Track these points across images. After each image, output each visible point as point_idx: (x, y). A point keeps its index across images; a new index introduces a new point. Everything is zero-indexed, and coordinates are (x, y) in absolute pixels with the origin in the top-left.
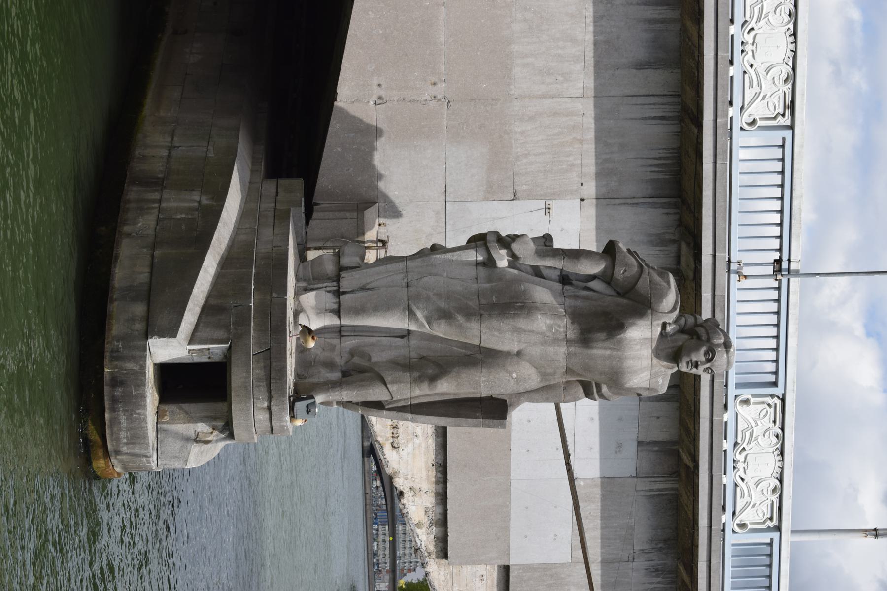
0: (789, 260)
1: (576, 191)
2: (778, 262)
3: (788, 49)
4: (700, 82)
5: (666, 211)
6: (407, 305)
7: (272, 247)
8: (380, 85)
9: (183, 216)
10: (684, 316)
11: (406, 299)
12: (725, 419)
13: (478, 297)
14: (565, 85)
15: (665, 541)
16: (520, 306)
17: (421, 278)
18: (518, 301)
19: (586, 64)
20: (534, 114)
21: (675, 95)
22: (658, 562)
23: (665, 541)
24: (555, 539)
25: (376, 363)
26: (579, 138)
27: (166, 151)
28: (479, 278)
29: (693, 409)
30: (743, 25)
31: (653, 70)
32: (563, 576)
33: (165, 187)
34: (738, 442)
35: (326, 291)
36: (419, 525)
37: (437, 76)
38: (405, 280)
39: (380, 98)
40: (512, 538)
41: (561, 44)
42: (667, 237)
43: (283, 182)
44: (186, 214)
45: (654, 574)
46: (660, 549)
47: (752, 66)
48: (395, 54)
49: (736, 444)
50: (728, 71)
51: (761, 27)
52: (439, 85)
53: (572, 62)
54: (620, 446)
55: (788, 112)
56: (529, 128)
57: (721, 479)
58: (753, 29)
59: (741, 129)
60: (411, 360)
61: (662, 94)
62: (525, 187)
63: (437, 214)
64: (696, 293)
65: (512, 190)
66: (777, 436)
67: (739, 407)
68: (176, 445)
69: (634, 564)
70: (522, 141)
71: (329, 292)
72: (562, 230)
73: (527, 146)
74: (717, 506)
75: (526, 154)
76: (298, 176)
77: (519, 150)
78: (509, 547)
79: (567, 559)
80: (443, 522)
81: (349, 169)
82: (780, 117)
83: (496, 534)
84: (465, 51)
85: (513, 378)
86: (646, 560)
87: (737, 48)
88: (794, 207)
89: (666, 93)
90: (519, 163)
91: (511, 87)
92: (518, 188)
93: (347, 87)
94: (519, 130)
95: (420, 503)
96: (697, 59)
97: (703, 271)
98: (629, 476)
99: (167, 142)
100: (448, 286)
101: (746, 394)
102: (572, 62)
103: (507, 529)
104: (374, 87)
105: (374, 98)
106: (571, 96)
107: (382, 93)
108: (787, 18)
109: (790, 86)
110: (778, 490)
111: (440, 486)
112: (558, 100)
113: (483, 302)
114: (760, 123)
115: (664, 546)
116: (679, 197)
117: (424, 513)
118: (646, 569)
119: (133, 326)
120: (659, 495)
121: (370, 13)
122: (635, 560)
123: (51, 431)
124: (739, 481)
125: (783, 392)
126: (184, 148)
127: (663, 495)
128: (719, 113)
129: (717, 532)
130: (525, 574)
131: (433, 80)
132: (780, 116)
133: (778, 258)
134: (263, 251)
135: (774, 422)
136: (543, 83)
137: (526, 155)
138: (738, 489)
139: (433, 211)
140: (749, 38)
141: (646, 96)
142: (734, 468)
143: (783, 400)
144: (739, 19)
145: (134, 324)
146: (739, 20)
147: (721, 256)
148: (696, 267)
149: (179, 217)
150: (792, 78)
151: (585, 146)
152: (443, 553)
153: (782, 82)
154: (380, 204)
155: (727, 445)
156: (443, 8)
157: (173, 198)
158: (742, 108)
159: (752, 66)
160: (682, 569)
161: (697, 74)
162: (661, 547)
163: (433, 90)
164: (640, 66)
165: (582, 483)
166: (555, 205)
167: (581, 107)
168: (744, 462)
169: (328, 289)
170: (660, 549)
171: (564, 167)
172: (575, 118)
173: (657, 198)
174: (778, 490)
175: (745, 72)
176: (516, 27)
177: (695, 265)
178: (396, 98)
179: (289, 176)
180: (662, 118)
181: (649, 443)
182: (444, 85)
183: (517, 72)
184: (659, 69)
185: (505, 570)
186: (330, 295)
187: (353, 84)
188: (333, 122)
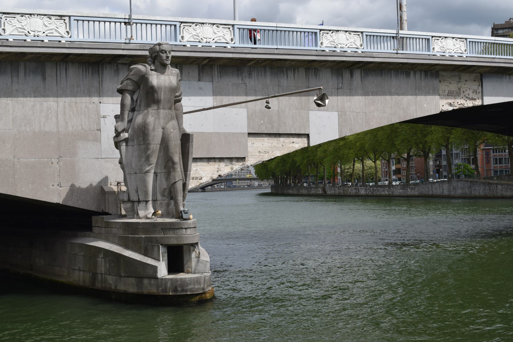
0: (277, 27)
2: (125, 23)
5: (105, 69)
8: (53, 185)
9: (108, 265)
11: (141, 174)
13: (140, 145)
14: (52, 109)
23: (238, 71)
26: (74, 104)
30: (27, 36)
32: (252, 111)
33: (96, 272)
36: (232, 169)
39: (58, 185)
41: (35, 111)
42: (115, 68)
45: (251, 75)
47: (44, 33)
49: (199, 42)
50: (46, 42)
51: (27, 28)
54: (200, 88)
55: (63, 18)
56: (70, 124)
58: (28, 32)
59: (70, 37)
62: (95, 126)
65: (96, 131)
71: (138, 205)
74: (59, 44)
76: (91, 218)
82: (65, 21)
89: (56, 68)
90: (85, 128)
92: (95, 129)
101: (179, 37)
103: (234, 134)
105: (58, 187)
107: (56, 184)
108: (24, 18)
109: (52, 17)
113: (142, 143)
114: (68, 30)
117: (227, 167)
121: (22, 189)
131: (50, 163)
134: (122, 232)
137: (82, 125)
140: (32, 33)
144: (24, 38)
148: (128, 57)
149: (108, 266)
150: (49, 16)
151: (78, 101)
153: (50, 20)
155: (200, 45)
158: (62, 37)
159: (44, 33)
160: (249, 64)
161: (48, 55)
164: (44, 79)
165: (215, 104)
166: (102, 114)
168: (35, 32)
169: (137, 205)
170: (241, 73)
171: (87, 110)
176: (28, 129)
178: (58, 179)
183: (47, 129)
185: (250, 134)
188: (68, 204)
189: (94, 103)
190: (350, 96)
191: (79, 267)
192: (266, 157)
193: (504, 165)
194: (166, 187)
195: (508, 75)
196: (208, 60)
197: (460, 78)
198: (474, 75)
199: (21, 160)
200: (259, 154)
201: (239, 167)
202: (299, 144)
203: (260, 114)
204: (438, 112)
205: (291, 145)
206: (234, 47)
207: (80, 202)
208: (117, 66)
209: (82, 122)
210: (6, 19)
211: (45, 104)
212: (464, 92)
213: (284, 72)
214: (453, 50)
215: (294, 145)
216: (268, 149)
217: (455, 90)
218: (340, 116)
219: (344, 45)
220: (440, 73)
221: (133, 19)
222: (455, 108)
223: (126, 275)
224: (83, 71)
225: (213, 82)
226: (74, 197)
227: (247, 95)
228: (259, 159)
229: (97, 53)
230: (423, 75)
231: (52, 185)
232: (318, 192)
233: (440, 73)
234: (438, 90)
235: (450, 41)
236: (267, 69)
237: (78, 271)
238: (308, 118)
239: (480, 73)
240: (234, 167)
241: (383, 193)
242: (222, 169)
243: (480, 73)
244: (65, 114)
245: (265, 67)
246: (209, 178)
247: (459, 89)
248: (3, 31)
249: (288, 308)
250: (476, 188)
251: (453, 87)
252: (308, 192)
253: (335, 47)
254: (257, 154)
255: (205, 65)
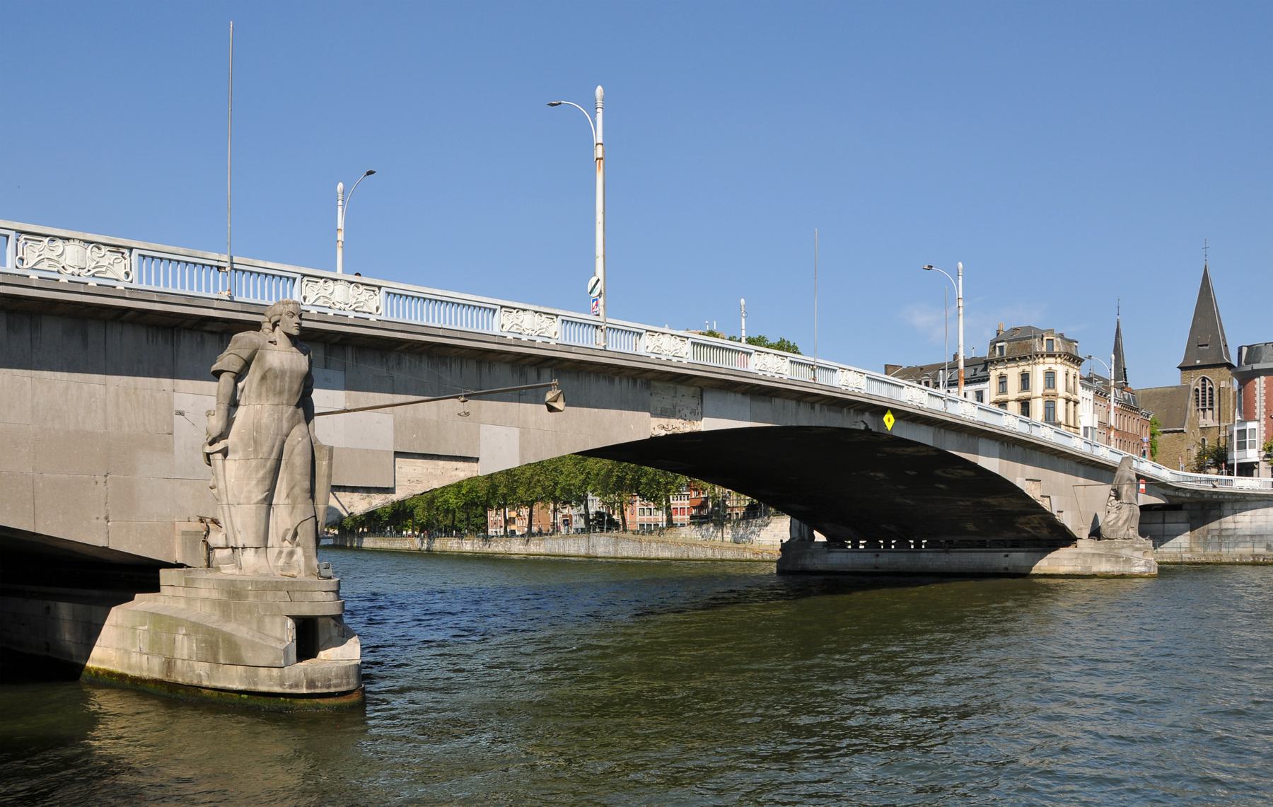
1: (168, 394)
5: (182, 337)
8: (98, 518)
9: (195, 645)
11: (249, 506)
12: (353, 317)
14: (98, 396)
25: (292, 526)
33: (173, 656)
36: (370, 503)
41: (69, 397)
42: (199, 339)
43: (162, 582)
44: (193, 643)
49: (330, 308)
52: (97, 480)
54: (326, 379)
55: (122, 250)
57: (539, 343)
58: (63, 267)
62: (165, 428)
65: (167, 436)
66: (326, 282)
67: (25, 266)
71: (242, 554)
72: (193, 405)
74: (110, 291)
76: (159, 573)
79: (391, 416)
80: (368, 490)
87: (76, 279)
103: (373, 451)
109: (102, 247)
110: (98, 245)
111: (347, 489)
113: (252, 456)
121: (48, 523)
123: (995, 675)
129: (132, 293)
134: (217, 595)
135: (511, 312)
142: (344, 310)
146: (56, 276)
152: (390, 490)
155: (331, 313)
156: (44, 474)
163: (101, 484)
165: (348, 404)
174: (98, 245)
175: (94, 276)
179: (158, 579)
180: (490, 367)
181: (326, 362)
185: (398, 454)
190: (536, 403)
192: (418, 488)
193: (645, 517)
195: (734, 392)
197: (676, 393)
198: (693, 389)
199: (45, 475)
202: (461, 472)
204: (649, 437)
205: (453, 473)
206: (380, 320)
207: (140, 546)
210: (26, 243)
211: (85, 387)
212: (679, 411)
213: (447, 364)
214: (349, 305)
215: (457, 473)
216: (421, 476)
217: (669, 407)
218: (522, 434)
219: (83, 272)
220: (653, 383)
222: (669, 433)
224: (148, 339)
226: (131, 537)
227: (393, 391)
230: (630, 381)
233: (653, 383)
234: (649, 406)
235: (850, 374)
236: (592, 375)
238: (479, 434)
239: (700, 387)
241: (497, 550)
242: (356, 504)
243: (700, 387)
245: (421, 354)
246: (336, 516)
247: (675, 407)
248: (21, 261)
249: (161, 768)
250: (624, 546)
251: (667, 403)
253: (520, 334)
254: (406, 484)
255: (336, 344)
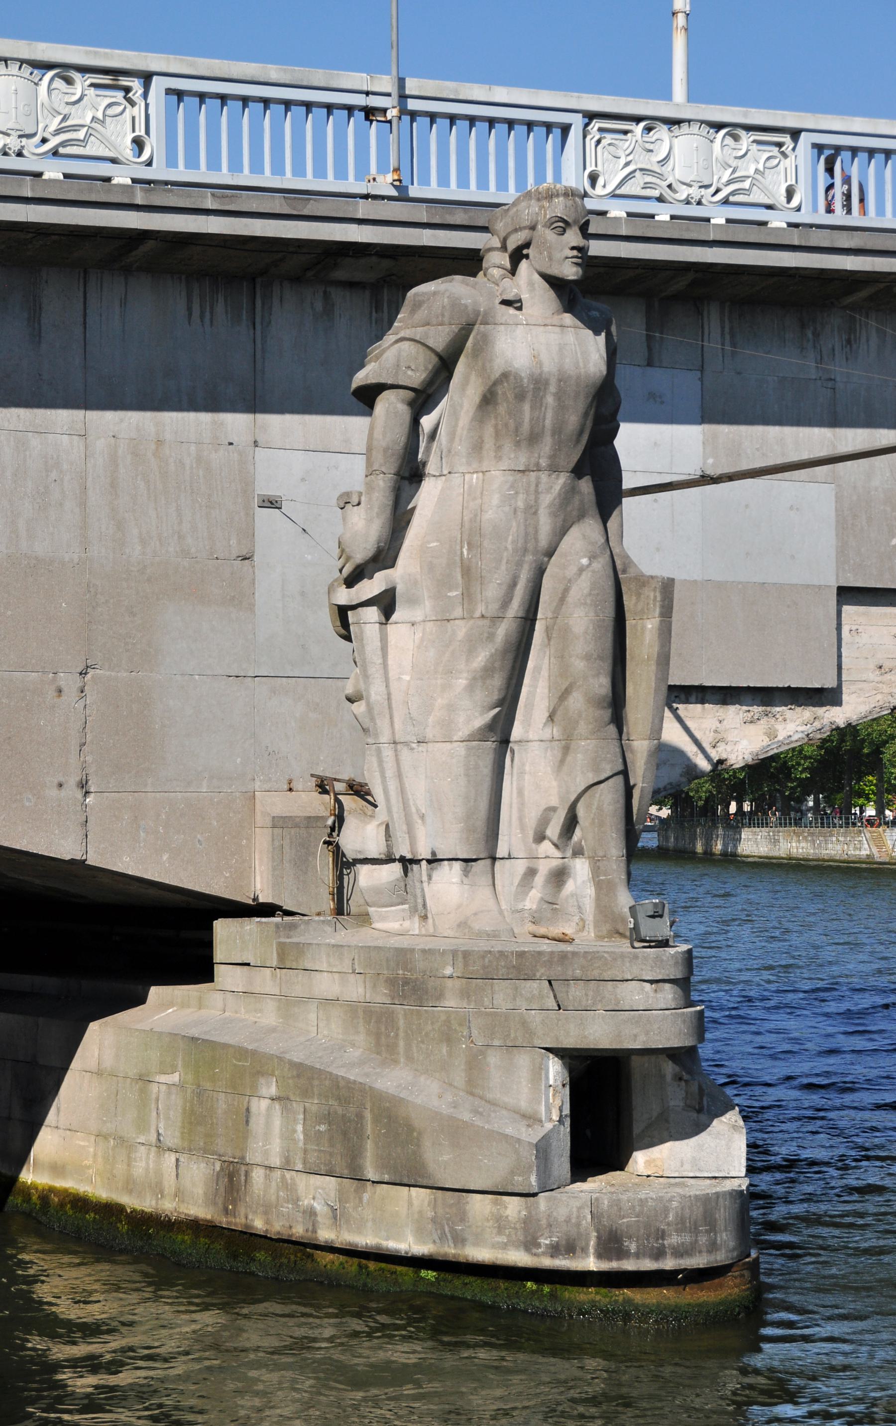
3: (18, 74)
4: (72, 231)
5: (276, 301)
6: (461, 744)
7: (353, 975)
9: (300, 1128)
10: (487, 269)
13: (448, 620)
14: (65, 467)
15: (803, 326)
16: (469, 549)
17: (411, 718)
18: (459, 553)
19: (31, 429)
20: (112, 522)
21: (85, 278)
22: (836, 340)
23: (803, 326)
24: (797, 509)
26: (153, 446)
27: (167, 1155)
28: (413, 619)
29: (602, 270)
31: (43, 315)
32: (855, 498)
33: (243, 1158)
34: (658, 195)
35: (429, 883)
36: (771, 734)
37: (47, 686)
38: (414, 745)
40: (794, 581)
42: (319, 306)
44: (295, 1121)
45: (855, 346)
46: (816, 335)
48: (8, 757)
49: (660, 199)
52: (62, 683)
53: (28, 453)
55: (125, 82)
56: (135, 531)
60: (556, 737)
61: (82, 300)
62: (233, 542)
63: (275, 693)
64: (419, 256)
65: (238, 563)
68: (706, 1145)
69: (838, 379)
70: (158, 543)
71: (430, 877)
73: (165, 535)
75: (179, 537)
76: (210, 928)
77: (171, 549)
78: (808, 586)
79: (828, 491)
81: (199, 841)
83: (788, 606)
84: (5, 637)
85: (590, 564)
86: (833, 360)
88: (282, 81)
89: (81, 294)
90: (193, 550)
91: (67, 560)
92: (234, 556)
93: (62, 842)
94: (139, 548)
95: (736, 731)
96: (31, 235)
97: (386, 242)
98: (700, 383)
99: (148, 1154)
100: (428, 672)
102: (28, 453)
104: (62, 795)
106: (83, 456)
112: (90, 479)
113: (458, 612)
114: (141, 131)
115: (812, 328)
116: (254, 279)
117: (752, 726)
118: (847, 359)
119: (510, 1218)
120: (732, 336)
122: (833, 377)
124: (720, 196)
125: (581, 115)
126: (161, 1125)
127: (731, 329)
128: (126, 201)
130: (852, 562)
131: (51, 693)
132: (130, 95)
133: (363, 113)
136: (61, 504)
137: (181, 537)
138: (732, 199)
139: (270, 699)
141: (85, 328)
142: (699, 203)
143: (591, 116)
145: (507, 1217)
147: (363, 209)
148: (377, 254)
149: (302, 1137)
154: (257, 788)
157: (264, 1146)
160: (849, 300)
161: (56, 237)
162: (813, 334)
163: (70, 693)
166: (264, 488)
167: (103, 440)
169: (425, 878)
170: (816, 335)
171: (201, 473)
172: (120, 452)
173: (254, 318)
177: (370, 255)
179: (209, 945)
182: (62, 675)
184: (40, 305)
186: (436, 875)
187: (57, 832)
189: (231, 444)
191: (159, 1134)
194: (554, 801)
196: (691, 276)
200: (879, 679)
201: (800, 729)
203: (888, 509)
208: (326, 296)
209: (180, 523)
214: (712, 190)
219: (30, 145)
221: (389, 95)
223: (386, 1178)
225: (702, 369)
228: (879, 697)
229: (258, 233)
231: (56, 782)
232: (855, 849)
237: (154, 1149)
240: (779, 727)
244: (113, 485)
252: (814, 849)
